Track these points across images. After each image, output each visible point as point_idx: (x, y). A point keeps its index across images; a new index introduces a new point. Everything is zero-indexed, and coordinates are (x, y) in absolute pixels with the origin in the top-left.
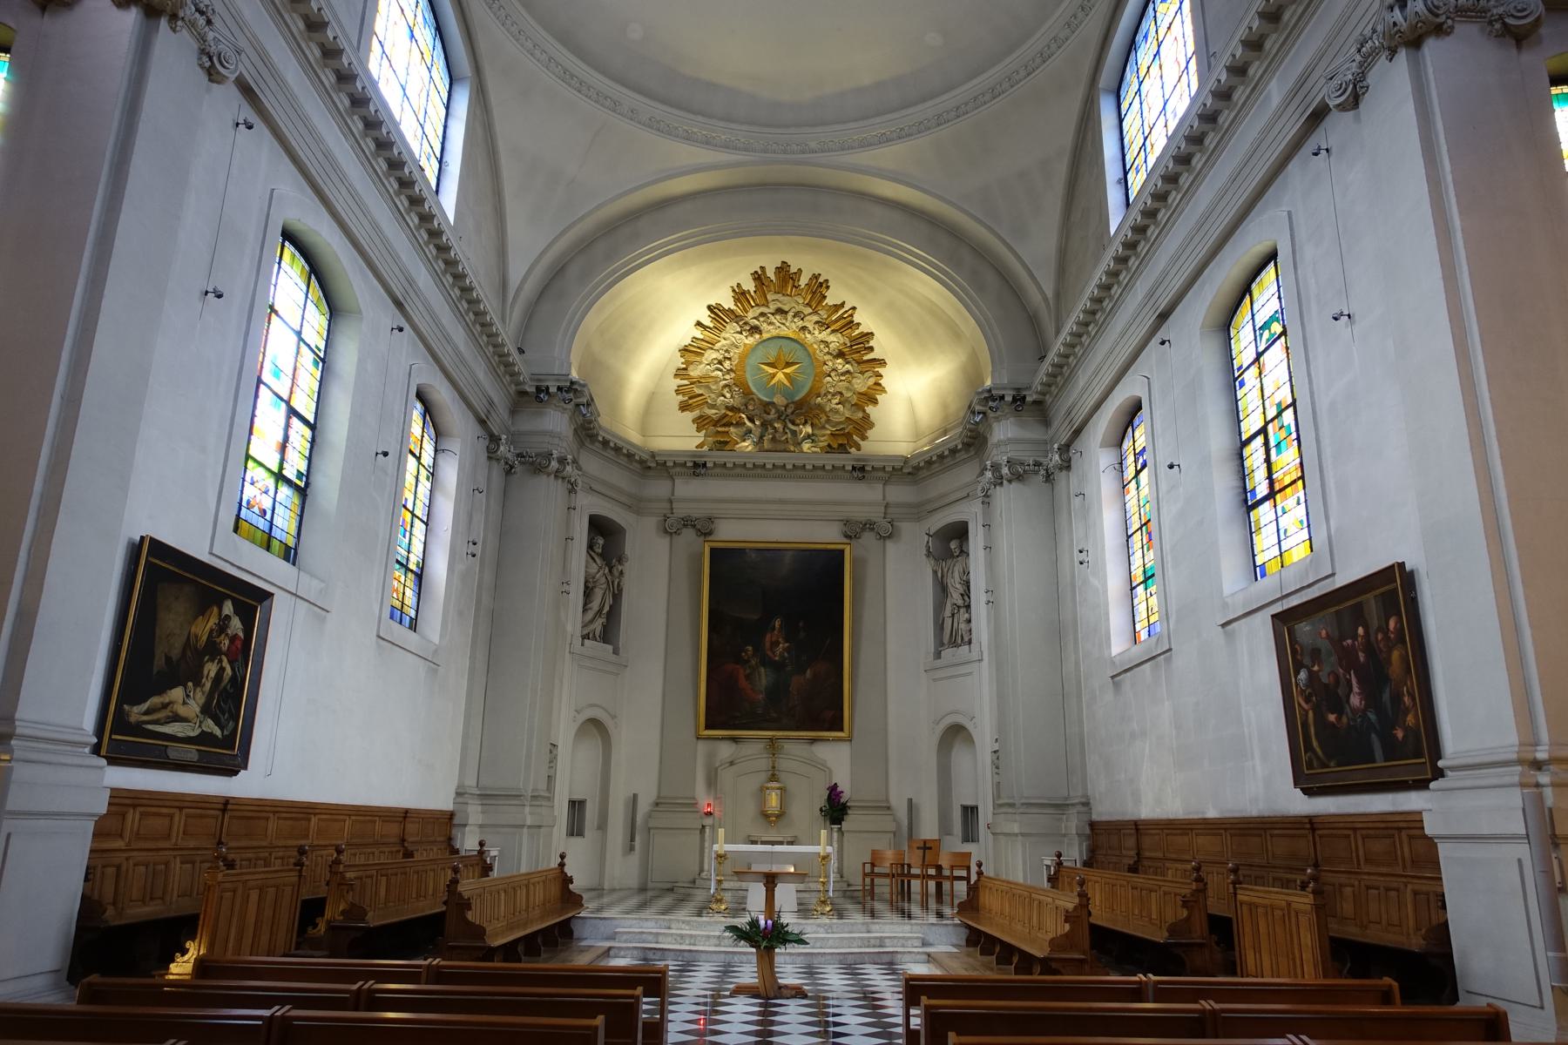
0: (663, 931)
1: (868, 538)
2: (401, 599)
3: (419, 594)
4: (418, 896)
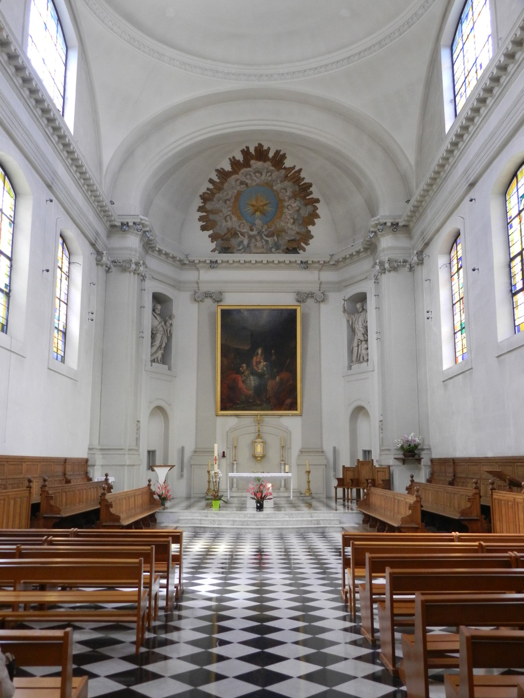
0: (203, 518)
1: (310, 302)
2: (56, 347)
3: (65, 343)
4: (80, 502)
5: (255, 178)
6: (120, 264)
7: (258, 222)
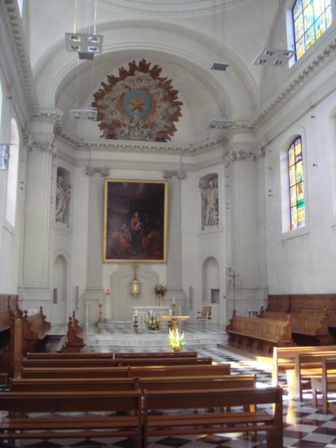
1: (174, 178)
5: (136, 84)
7: (136, 117)
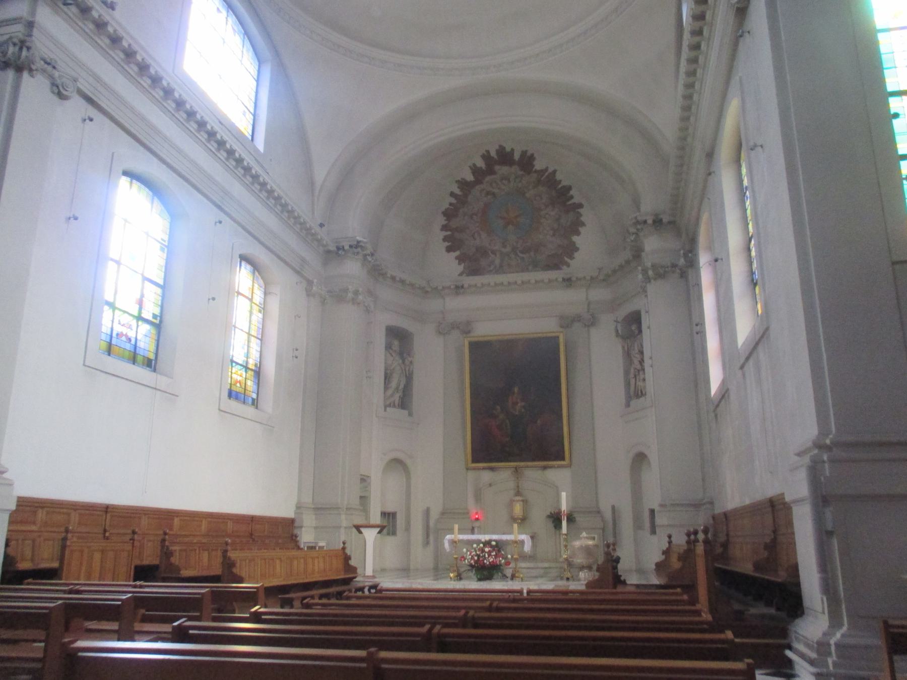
6: (336, 293)
